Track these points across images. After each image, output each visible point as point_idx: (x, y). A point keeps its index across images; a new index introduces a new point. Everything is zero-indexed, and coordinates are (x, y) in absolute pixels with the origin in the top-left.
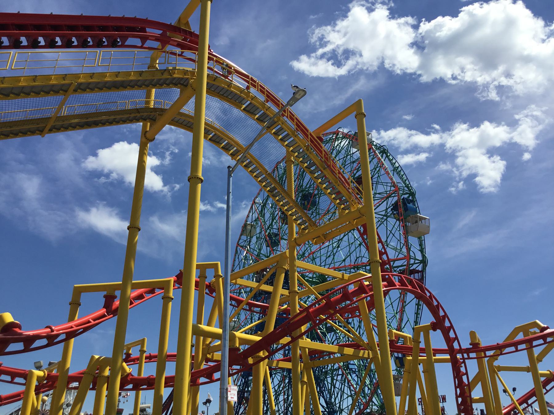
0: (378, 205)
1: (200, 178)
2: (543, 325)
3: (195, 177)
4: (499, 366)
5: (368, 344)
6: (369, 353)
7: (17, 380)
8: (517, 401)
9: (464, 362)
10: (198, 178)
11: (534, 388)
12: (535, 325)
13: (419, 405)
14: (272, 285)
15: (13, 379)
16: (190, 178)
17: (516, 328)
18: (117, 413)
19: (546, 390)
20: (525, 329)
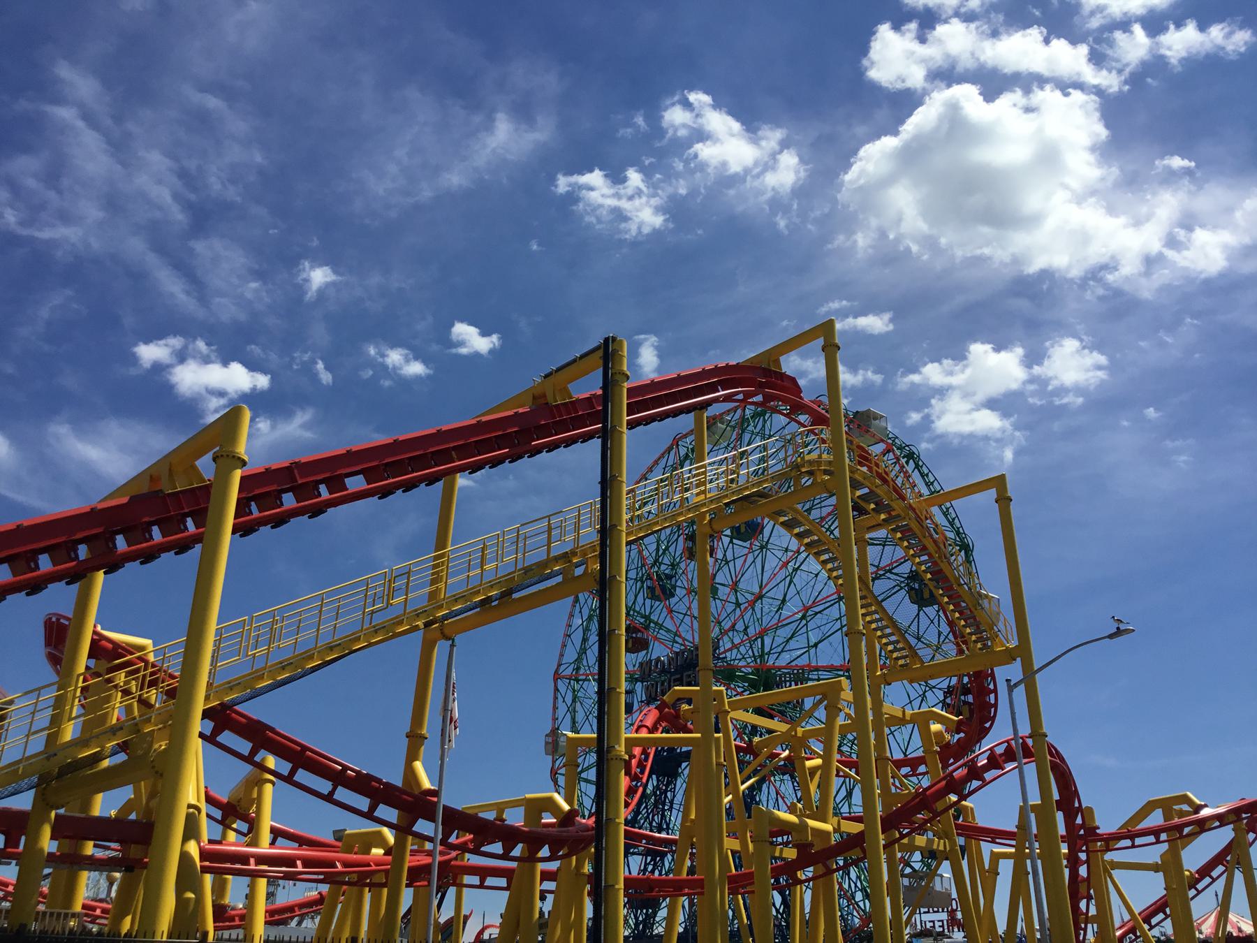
0: (902, 560)
1: (239, 458)
2: (1198, 802)
3: (228, 456)
4: (1112, 861)
5: (1238, 863)
6: (945, 843)
7: (490, 881)
8: (1140, 914)
9: (249, 759)
10: (234, 457)
11: (1165, 896)
12: (1185, 799)
13: (339, 835)
14: (1016, 761)
15: (482, 880)
16: (218, 456)
17: (1149, 802)
18: (730, 940)
19: (332, 793)
20: (1166, 805)
